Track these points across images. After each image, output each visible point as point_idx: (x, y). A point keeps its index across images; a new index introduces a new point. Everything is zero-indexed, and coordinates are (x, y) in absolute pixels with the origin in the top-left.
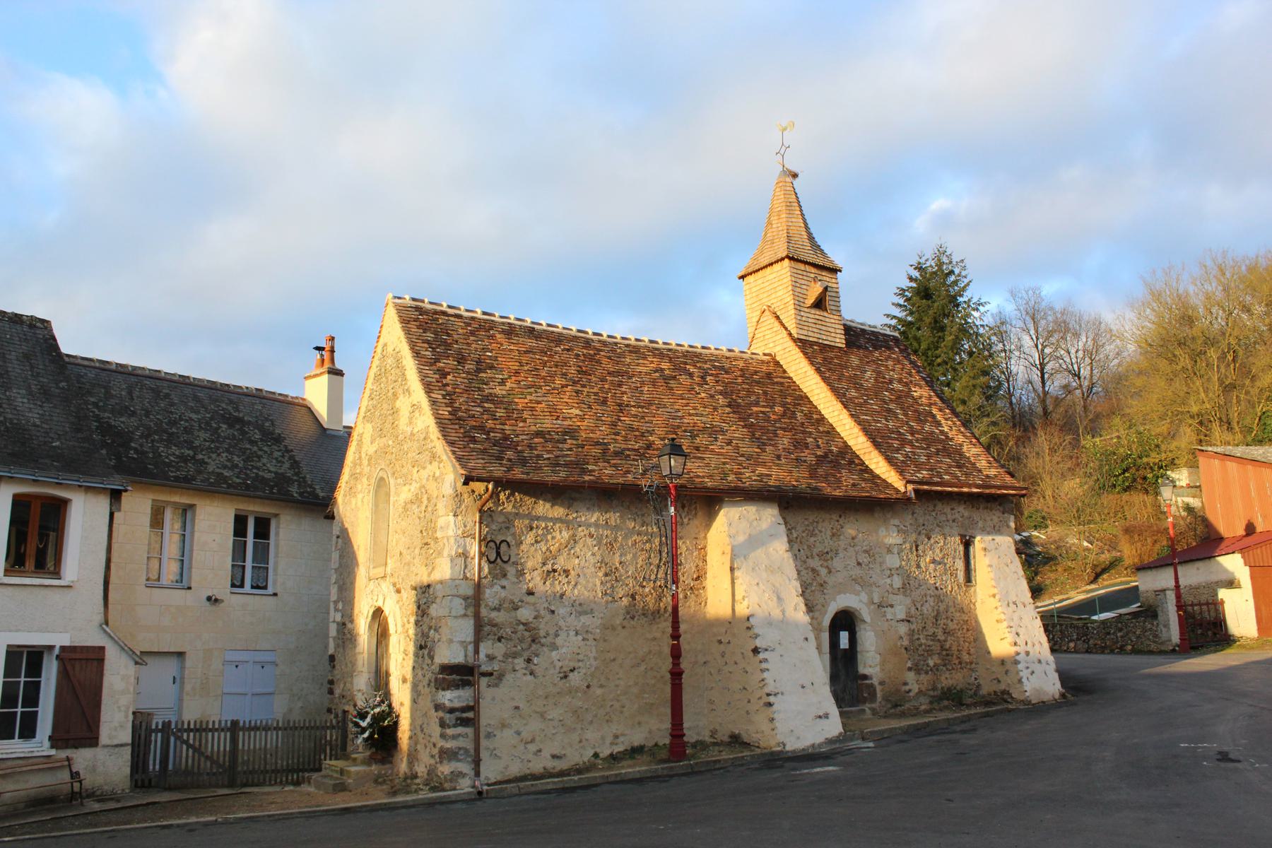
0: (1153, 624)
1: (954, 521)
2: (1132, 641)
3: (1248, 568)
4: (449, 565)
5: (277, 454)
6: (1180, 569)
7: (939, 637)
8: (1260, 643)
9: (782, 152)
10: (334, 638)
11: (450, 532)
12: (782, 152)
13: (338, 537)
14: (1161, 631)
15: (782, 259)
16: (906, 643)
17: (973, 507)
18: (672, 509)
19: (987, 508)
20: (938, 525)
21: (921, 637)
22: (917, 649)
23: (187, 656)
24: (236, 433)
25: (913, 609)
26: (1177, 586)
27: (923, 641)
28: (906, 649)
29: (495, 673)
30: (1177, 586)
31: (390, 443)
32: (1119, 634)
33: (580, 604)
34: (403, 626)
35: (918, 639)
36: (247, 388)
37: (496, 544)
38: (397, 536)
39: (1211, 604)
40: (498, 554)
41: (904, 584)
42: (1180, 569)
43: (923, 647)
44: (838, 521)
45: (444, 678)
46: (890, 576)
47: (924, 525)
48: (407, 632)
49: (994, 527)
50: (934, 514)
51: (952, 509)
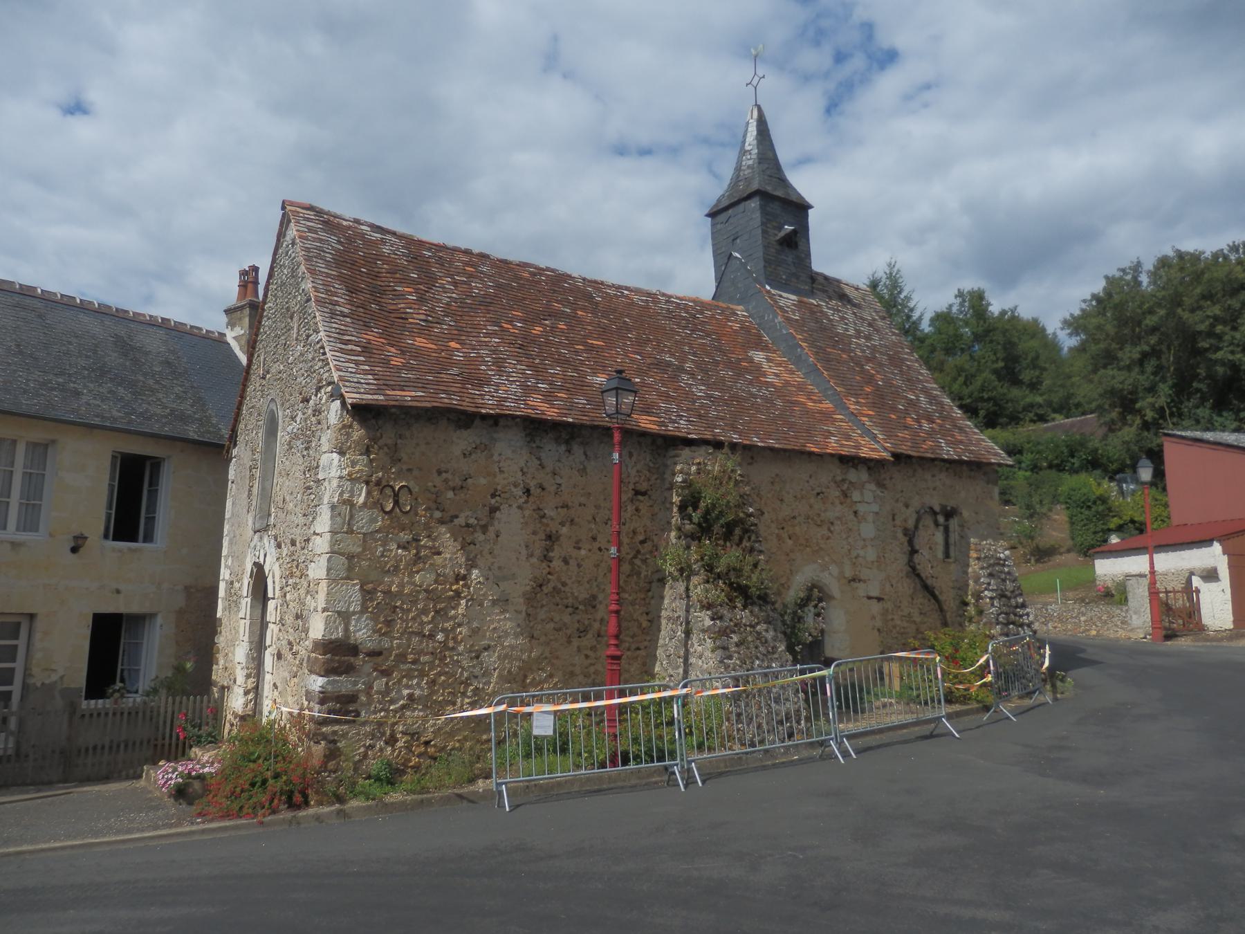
0: (1122, 610)
1: (934, 489)
2: (1097, 626)
3: (1226, 557)
4: (329, 514)
5: (178, 389)
6: (1156, 556)
7: (915, 619)
8: (1233, 635)
9: (755, 83)
10: (223, 599)
11: (334, 473)
12: (755, 83)
13: (232, 482)
14: (1131, 617)
15: (749, 197)
16: (879, 623)
17: (955, 475)
18: (616, 456)
19: (970, 477)
20: (918, 494)
21: (895, 617)
22: (891, 631)
23: (109, 607)
24: (128, 363)
25: (888, 586)
26: (1153, 572)
27: (899, 622)
28: (879, 630)
29: (384, 652)
30: (1153, 572)
31: (282, 367)
32: (1083, 619)
33: (500, 568)
34: (282, 588)
35: (892, 619)
36: (151, 316)
37: (394, 490)
38: (280, 480)
39: (1170, 592)
40: (396, 503)
41: (879, 557)
42: (1156, 556)
43: (898, 628)
44: (808, 482)
45: (316, 658)
46: (864, 547)
47: (902, 491)
48: (285, 596)
49: (977, 498)
50: (913, 480)
51: (933, 476)
